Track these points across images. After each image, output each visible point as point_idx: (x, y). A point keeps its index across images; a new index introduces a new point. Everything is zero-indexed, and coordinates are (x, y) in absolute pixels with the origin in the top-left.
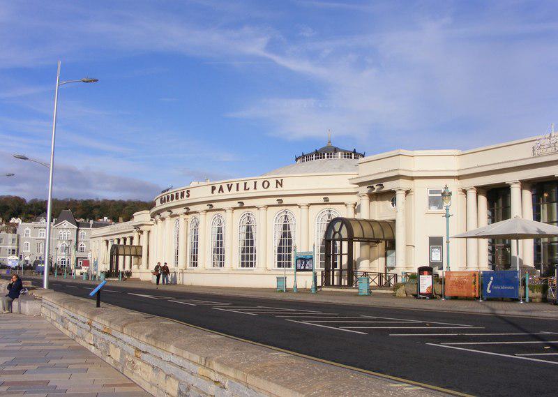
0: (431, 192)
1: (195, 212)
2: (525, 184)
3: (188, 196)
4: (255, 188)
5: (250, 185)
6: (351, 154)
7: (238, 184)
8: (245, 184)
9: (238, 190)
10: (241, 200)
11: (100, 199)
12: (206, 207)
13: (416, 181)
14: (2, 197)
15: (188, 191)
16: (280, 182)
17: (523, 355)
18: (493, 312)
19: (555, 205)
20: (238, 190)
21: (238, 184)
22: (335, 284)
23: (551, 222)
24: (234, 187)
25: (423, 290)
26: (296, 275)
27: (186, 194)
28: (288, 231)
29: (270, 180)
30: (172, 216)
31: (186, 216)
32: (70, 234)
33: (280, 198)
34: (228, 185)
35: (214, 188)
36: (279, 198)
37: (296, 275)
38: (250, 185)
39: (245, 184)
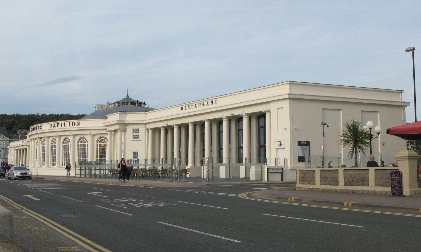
3: (41, 129)
4: (69, 125)
5: (67, 124)
6: (136, 103)
7: (61, 123)
8: (65, 123)
9: (61, 126)
11: (40, 114)
13: (272, 104)
14: (4, 116)
15: (41, 126)
16: (78, 125)
17: (337, 206)
19: (202, 177)
20: (61, 126)
21: (61, 123)
23: (213, 182)
25: (418, 146)
27: (40, 128)
29: (75, 122)
32: (5, 143)
34: (57, 124)
35: (51, 125)
39: (65, 123)
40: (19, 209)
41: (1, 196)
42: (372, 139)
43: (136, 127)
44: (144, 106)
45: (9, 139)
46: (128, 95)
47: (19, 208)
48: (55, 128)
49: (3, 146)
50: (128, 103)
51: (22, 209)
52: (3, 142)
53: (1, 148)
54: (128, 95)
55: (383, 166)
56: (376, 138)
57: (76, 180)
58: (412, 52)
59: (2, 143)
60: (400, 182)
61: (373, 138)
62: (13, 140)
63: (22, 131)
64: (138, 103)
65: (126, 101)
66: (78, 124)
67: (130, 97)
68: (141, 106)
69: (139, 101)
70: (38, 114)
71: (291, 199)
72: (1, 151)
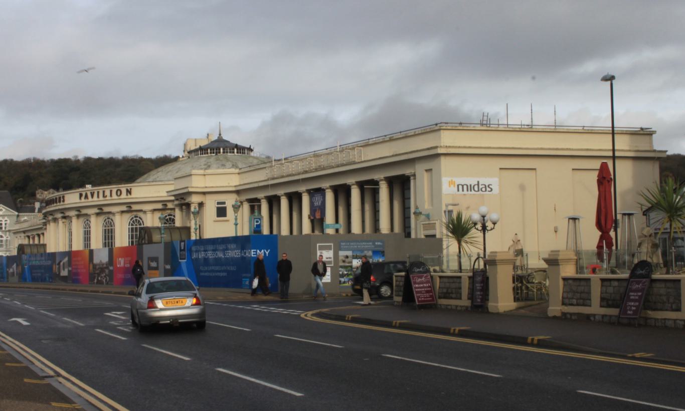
0: (218, 203)
1: (110, 213)
2: (309, 192)
3: (64, 201)
5: (107, 193)
10: (100, 207)
12: (96, 210)
14: (8, 165)
15: (63, 197)
18: (642, 144)
22: (34, 274)
24: (96, 195)
26: (614, 150)
27: (62, 199)
28: (130, 227)
29: (122, 189)
30: (64, 217)
31: (64, 220)
33: (129, 205)
34: (91, 193)
35: (81, 195)
36: (99, 207)
37: (614, 150)
38: (107, 193)
40: (52, 377)
41: (4, 335)
42: (486, 231)
43: (221, 198)
44: (249, 154)
45: (17, 213)
46: (220, 135)
47: (52, 373)
48: (86, 200)
49: (5, 228)
50: (220, 150)
51: (59, 375)
52: (6, 218)
53: (3, 231)
54: (220, 135)
55: (461, 272)
56: (491, 229)
57: (100, 291)
58: (609, 82)
59: (3, 220)
60: (428, 290)
61: (488, 230)
62: (23, 214)
63: (46, 192)
64: (237, 150)
65: (216, 145)
66: (129, 192)
67: (225, 138)
68: (243, 153)
69: (240, 143)
70: (76, 157)
71: (454, 330)
72: (2, 237)
